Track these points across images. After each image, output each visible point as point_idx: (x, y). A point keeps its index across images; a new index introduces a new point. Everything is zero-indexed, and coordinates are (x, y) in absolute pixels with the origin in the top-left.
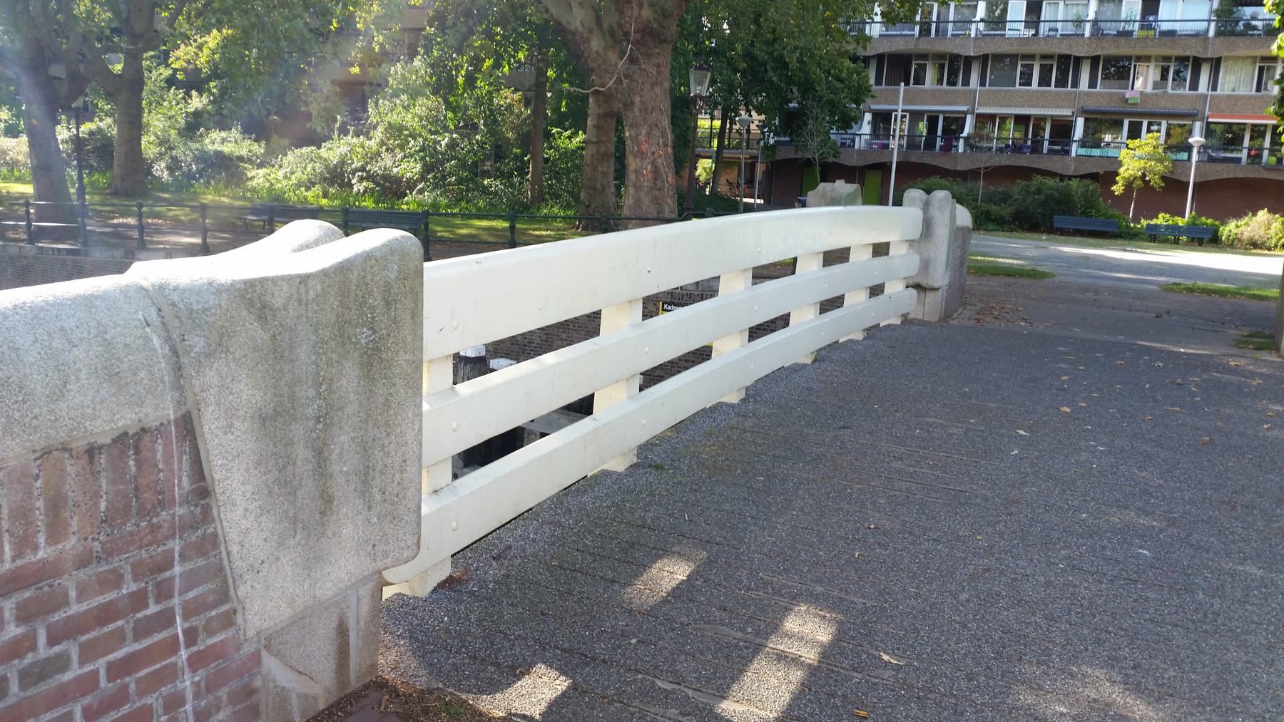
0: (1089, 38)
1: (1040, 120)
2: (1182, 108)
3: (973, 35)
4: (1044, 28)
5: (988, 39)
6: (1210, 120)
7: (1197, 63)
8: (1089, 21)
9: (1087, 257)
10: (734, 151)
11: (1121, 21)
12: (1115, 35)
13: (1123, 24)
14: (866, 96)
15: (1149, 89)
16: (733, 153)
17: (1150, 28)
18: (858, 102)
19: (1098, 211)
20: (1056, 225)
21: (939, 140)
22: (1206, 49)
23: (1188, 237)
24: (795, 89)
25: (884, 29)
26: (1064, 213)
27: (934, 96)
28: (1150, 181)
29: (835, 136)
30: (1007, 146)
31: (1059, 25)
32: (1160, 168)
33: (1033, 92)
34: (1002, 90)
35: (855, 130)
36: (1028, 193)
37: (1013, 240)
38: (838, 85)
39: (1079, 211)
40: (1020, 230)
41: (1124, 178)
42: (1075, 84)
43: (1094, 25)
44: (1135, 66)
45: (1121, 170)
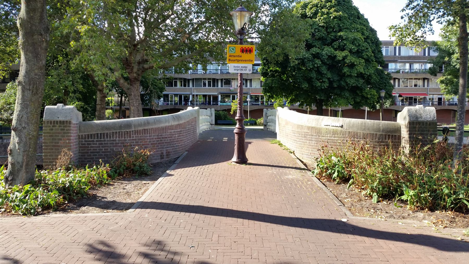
1: (209, 96)
4: (208, 72)
5: (194, 74)
20: (218, 123)
21: (183, 102)
31: (212, 71)
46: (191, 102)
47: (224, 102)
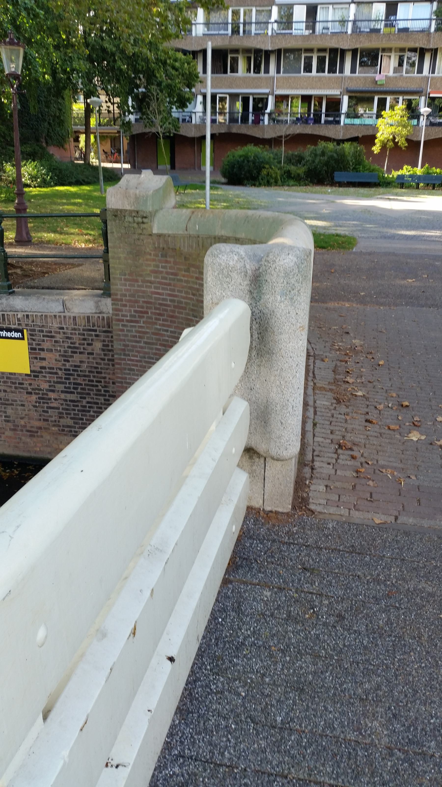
0: (351, 35)
1: (320, 99)
2: (413, 87)
3: (270, 33)
4: (319, 27)
5: (281, 37)
6: (431, 95)
7: (422, 52)
8: (350, 21)
9: (367, 210)
10: (106, 127)
11: (371, 21)
12: (367, 32)
13: (373, 23)
14: (195, 81)
15: (391, 74)
16: (104, 129)
17: (392, 26)
18: (190, 86)
19: (364, 167)
20: (337, 179)
21: (250, 115)
22: (429, 41)
23: (424, 184)
24: (141, 76)
25: (206, 29)
26: (340, 170)
27: (245, 82)
28: (398, 142)
29: (175, 113)
30: (298, 119)
31: (330, 25)
32: (405, 132)
33: (313, 77)
34: (292, 77)
35: (190, 107)
36: (316, 155)
37: (309, 195)
38: (174, 72)
39: (351, 168)
40: (311, 184)
41: (380, 141)
42: (341, 71)
43: (354, 24)
44: (382, 56)
45: (378, 135)
46: (270, 114)
47: (357, 116)
